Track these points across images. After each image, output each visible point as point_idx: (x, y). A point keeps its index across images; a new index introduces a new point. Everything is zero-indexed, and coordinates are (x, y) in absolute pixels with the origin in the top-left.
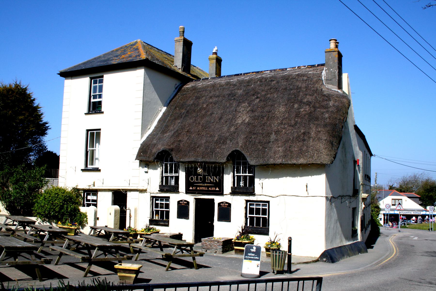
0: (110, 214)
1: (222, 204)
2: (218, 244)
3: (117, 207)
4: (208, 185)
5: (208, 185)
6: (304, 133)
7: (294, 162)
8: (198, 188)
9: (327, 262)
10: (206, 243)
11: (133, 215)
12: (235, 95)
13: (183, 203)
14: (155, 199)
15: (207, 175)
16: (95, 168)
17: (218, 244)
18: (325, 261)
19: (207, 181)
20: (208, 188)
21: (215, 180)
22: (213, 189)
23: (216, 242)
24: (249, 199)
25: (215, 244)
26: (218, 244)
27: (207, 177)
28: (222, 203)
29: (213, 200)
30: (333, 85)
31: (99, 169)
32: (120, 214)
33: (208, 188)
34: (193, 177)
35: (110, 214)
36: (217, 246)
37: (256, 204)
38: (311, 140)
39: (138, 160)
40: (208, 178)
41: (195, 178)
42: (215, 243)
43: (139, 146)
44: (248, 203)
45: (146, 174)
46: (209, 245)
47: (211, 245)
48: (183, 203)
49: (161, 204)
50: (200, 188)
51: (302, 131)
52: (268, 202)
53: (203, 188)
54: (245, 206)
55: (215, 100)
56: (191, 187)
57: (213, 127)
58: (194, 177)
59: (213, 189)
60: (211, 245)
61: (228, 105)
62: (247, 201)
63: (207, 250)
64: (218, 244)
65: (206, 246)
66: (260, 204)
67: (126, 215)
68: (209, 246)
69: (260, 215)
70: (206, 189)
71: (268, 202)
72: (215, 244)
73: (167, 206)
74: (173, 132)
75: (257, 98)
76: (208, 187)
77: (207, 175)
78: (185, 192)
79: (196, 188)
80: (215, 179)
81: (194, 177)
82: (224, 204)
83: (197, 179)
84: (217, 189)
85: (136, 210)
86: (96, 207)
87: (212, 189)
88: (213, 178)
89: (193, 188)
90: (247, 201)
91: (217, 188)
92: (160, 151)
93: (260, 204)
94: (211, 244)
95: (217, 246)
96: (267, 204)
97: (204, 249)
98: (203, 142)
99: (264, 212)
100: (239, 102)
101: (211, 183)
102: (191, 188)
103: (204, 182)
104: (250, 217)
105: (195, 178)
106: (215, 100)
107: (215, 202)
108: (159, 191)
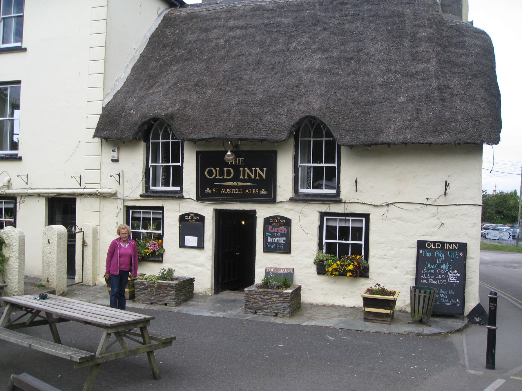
0: (49, 242)
1: (187, 217)
2: (280, 299)
3: (60, 229)
4: (245, 184)
5: (245, 184)
6: (440, 89)
7: (430, 139)
8: (223, 191)
9: (483, 324)
10: (254, 298)
11: (89, 241)
12: (279, 25)
13: (192, 219)
14: (132, 212)
15: (241, 166)
16: (9, 155)
17: (280, 299)
18: (479, 323)
19: (241, 177)
20: (244, 190)
21: (260, 175)
22: (255, 191)
23: (276, 296)
24: (328, 211)
25: (274, 299)
26: (282, 299)
27: (241, 169)
28: (188, 214)
29: (254, 212)
30: (454, 15)
31: (19, 156)
32: (68, 241)
33: (244, 190)
34: (212, 170)
35: (49, 242)
36: (278, 303)
37: (339, 219)
38: (457, 100)
39: (99, 137)
40: (244, 171)
41: (216, 172)
42: (274, 298)
43: (100, 112)
44: (325, 218)
45: (115, 164)
46: (262, 301)
47: (267, 301)
48: (192, 219)
49: (144, 219)
50: (226, 191)
51: (434, 85)
52: (367, 216)
53: (233, 191)
54: (317, 223)
55: (239, 32)
56: (208, 189)
57: (247, 77)
58: (216, 170)
59: (255, 191)
60: (267, 301)
61: (268, 41)
62: (323, 215)
63: (257, 311)
64: (282, 299)
65: (255, 302)
66: (151, 212)
67: (75, 241)
68: (262, 303)
69: (336, 240)
70: (239, 191)
71: (367, 216)
72: (274, 299)
73: (159, 223)
74: (166, 87)
75: (325, 29)
76: (244, 188)
77: (241, 166)
78: (194, 197)
79: (220, 190)
80: (259, 173)
81: (216, 170)
82: (276, 221)
83: (221, 173)
84: (263, 192)
85: (95, 232)
86: (15, 227)
87: (252, 191)
88: (256, 171)
89: (212, 191)
90: (323, 215)
91: (263, 190)
92: (146, 119)
93: (151, 212)
94: (266, 299)
95: (278, 303)
96: (364, 219)
97: (250, 308)
98: (234, 103)
99: (357, 233)
100: (291, 36)
101: (250, 180)
102: (208, 191)
103: (236, 178)
104: (326, 243)
105: (216, 172)
106: (239, 32)
107: (258, 215)
108: (141, 196)
